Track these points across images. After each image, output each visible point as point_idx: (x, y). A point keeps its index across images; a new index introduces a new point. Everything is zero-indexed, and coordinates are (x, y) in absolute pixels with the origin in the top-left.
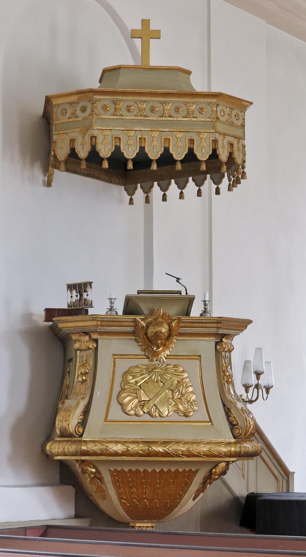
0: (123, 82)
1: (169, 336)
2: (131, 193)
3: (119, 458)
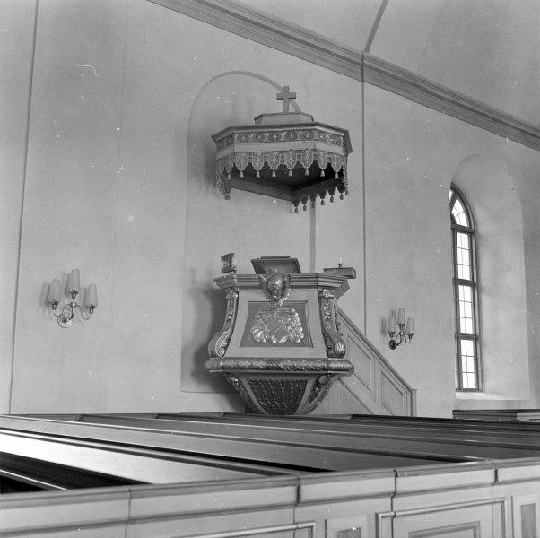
0: (265, 121)
1: (284, 288)
2: (296, 205)
3: (246, 371)
